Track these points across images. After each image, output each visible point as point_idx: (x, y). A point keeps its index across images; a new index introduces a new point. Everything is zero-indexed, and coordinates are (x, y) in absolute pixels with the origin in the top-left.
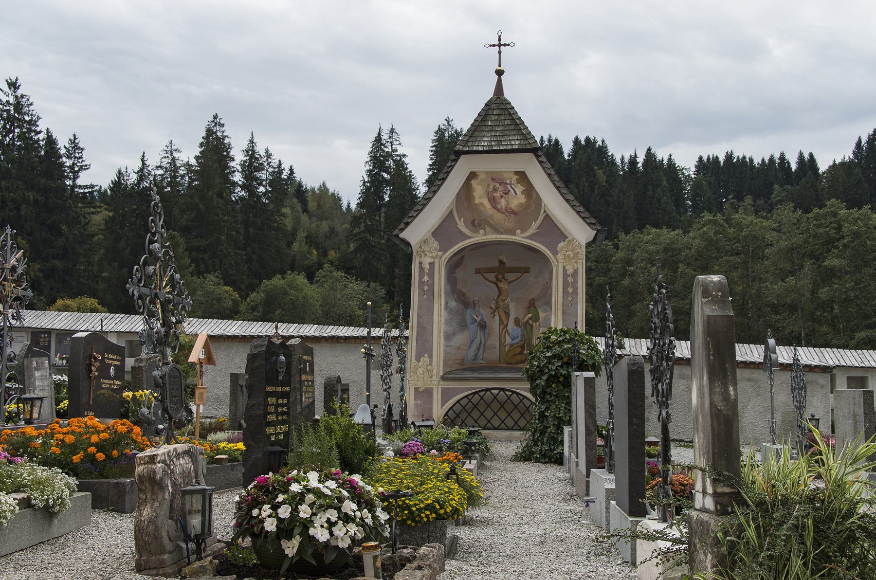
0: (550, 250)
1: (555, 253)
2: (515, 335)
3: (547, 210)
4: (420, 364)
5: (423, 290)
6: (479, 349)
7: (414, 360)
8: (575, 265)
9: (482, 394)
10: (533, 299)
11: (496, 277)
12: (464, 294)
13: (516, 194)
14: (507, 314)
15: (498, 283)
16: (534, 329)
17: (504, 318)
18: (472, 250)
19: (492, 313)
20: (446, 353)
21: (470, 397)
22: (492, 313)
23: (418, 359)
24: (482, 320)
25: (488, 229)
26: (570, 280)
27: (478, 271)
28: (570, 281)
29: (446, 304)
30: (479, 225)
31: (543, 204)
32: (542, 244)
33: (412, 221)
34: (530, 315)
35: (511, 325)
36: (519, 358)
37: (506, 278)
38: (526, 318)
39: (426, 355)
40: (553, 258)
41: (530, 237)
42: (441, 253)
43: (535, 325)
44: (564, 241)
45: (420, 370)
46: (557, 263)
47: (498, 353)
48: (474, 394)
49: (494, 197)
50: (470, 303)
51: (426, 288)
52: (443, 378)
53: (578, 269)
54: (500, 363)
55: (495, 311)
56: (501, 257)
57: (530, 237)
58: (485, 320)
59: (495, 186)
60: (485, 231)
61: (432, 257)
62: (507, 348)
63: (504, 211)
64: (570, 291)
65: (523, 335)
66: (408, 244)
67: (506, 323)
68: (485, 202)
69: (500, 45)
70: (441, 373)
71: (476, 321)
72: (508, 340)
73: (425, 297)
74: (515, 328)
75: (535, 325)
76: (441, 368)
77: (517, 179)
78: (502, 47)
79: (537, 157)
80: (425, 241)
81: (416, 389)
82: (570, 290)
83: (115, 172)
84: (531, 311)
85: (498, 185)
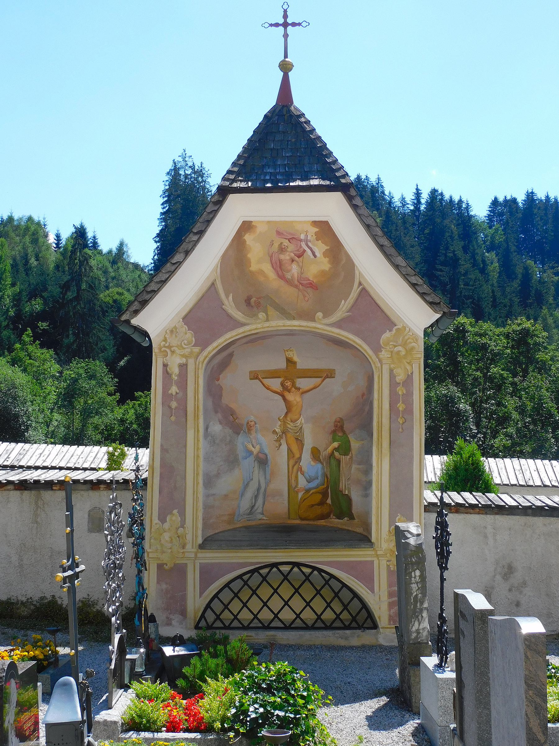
0: (368, 345)
1: (377, 349)
2: (313, 474)
3: (363, 282)
4: (166, 526)
5: (170, 407)
6: (256, 497)
7: (156, 520)
8: (408, 367)
9: (264, 571)
10: (341, 419)
11: (282, 384)
12: (232, 413)
13: (315, 256)
14: (300, 442)
15: (286, 394)
16: (343, 465)
17: (295, 448)
18: (247, 343)
19: (276, 441)
20: (207, 507)
21: (246, 577)
22: (276, 441)
23: (162, 519)
24: (261, 451)
25: (271, 311)
26: (401, 391)
27: (255, 376)
28: (400, 393)
29: (207, 428)
30: (258, 305)
31: (357, 272)
32: (357, 334)
33: (151, 299)
34: (336, 444)
35: (306, 457)
36: (319, 510)
37: (298, 385)
38: (330, 449)
39: (175, 512)
40: (374, 357)
41: (339, 324)
42: (197, 350)
43: (344, 459)
44: (390, 331)
45: (166, 536)
46: (379, 365)
47: (286, 502)
48: (252, 572)
49: (280, 261)
50: (242, 425)
51: (174, 404)
52: (202, 547)
53: (412, 373)
54: (289, 518)
55: (281, 437)
56: (290, 354)
57: (339, 324)
58: (266, 451)
59: (281, 243)
60: (267, 314)
61: (183, 356)
62: (300, 495)
63: (296, 282)
64: (401, 409)
65: (325, 475)
66: (145, 334)
67: (297, 455)
68: (267, 268)
69: (285, 25)
70: (200, 541)
71: (251, 453)
72: (302, 482)
73: (173, 418)
74: (312, 463)
75: (344, 459)
76: (200, 533)
77: (316, 234)
78: (289, 28)
79: (350, 198)
80: (173, 331)
81: (160, 567)
82: (401, 407)
83: (172, 163)
84: (337, 438)
85: (286, 243)
